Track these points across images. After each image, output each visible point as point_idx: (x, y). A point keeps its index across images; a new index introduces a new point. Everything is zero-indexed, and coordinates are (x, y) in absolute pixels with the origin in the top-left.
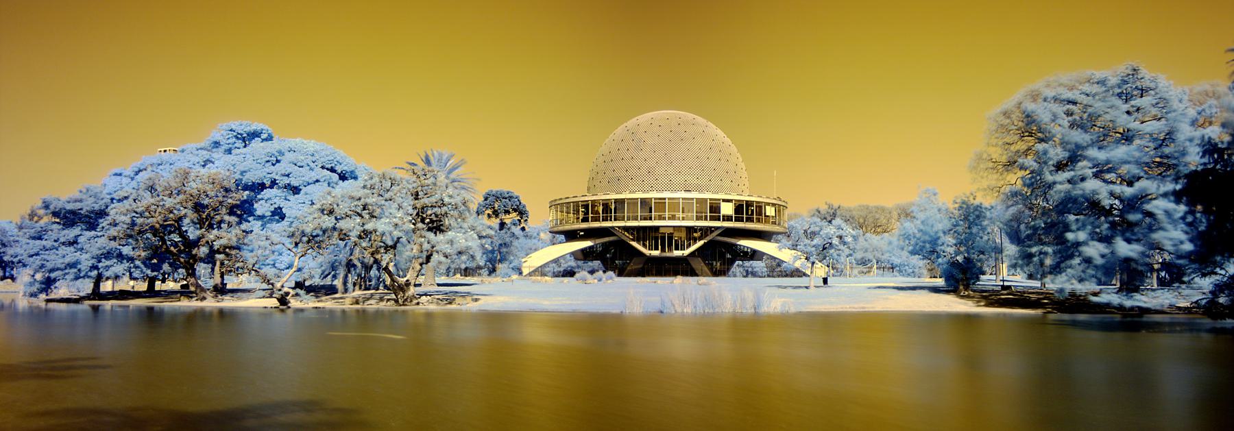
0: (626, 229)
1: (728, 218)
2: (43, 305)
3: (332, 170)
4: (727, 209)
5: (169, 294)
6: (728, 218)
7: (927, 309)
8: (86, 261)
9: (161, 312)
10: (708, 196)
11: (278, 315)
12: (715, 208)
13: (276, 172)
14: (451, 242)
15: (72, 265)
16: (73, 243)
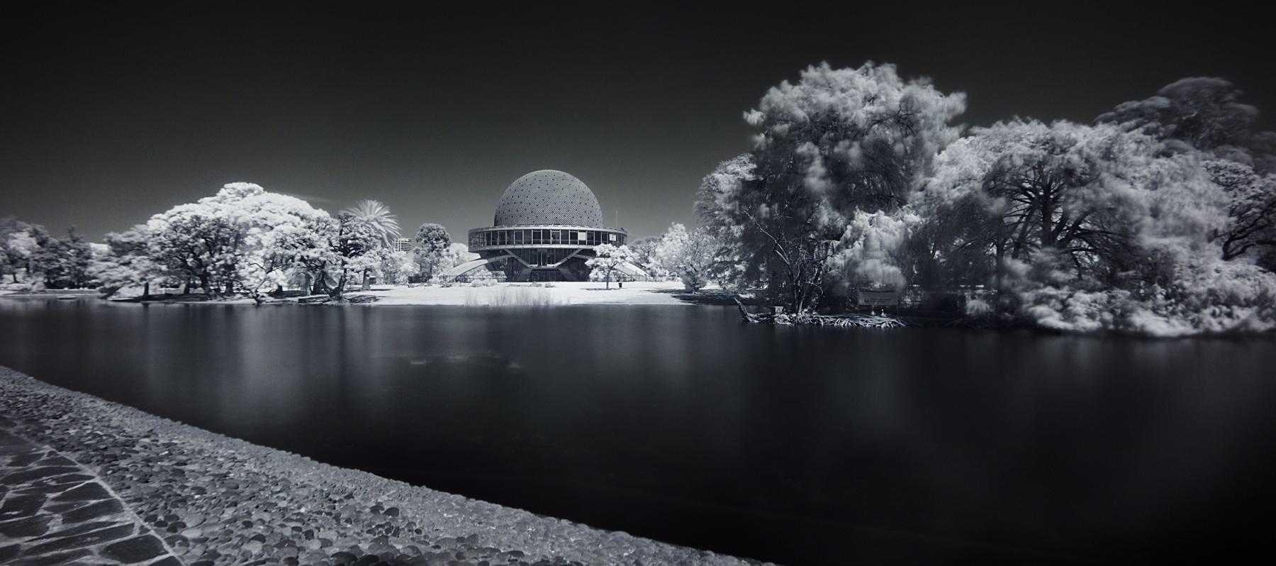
0: (512, 250)
1: (582, 243)
2: (112, 304)
3: (296, 214)
4: (582, 237)
5: (196, 296)
6: (582, 243)
7: (574, 302)
8: (135, 275)
9: (369, 307)
10: (569, 228)
11: (252, 312)
12: (574, 235)
13: (257, 216)
14: (360, 263)
15: (126, 278)
16: (128, 264)
